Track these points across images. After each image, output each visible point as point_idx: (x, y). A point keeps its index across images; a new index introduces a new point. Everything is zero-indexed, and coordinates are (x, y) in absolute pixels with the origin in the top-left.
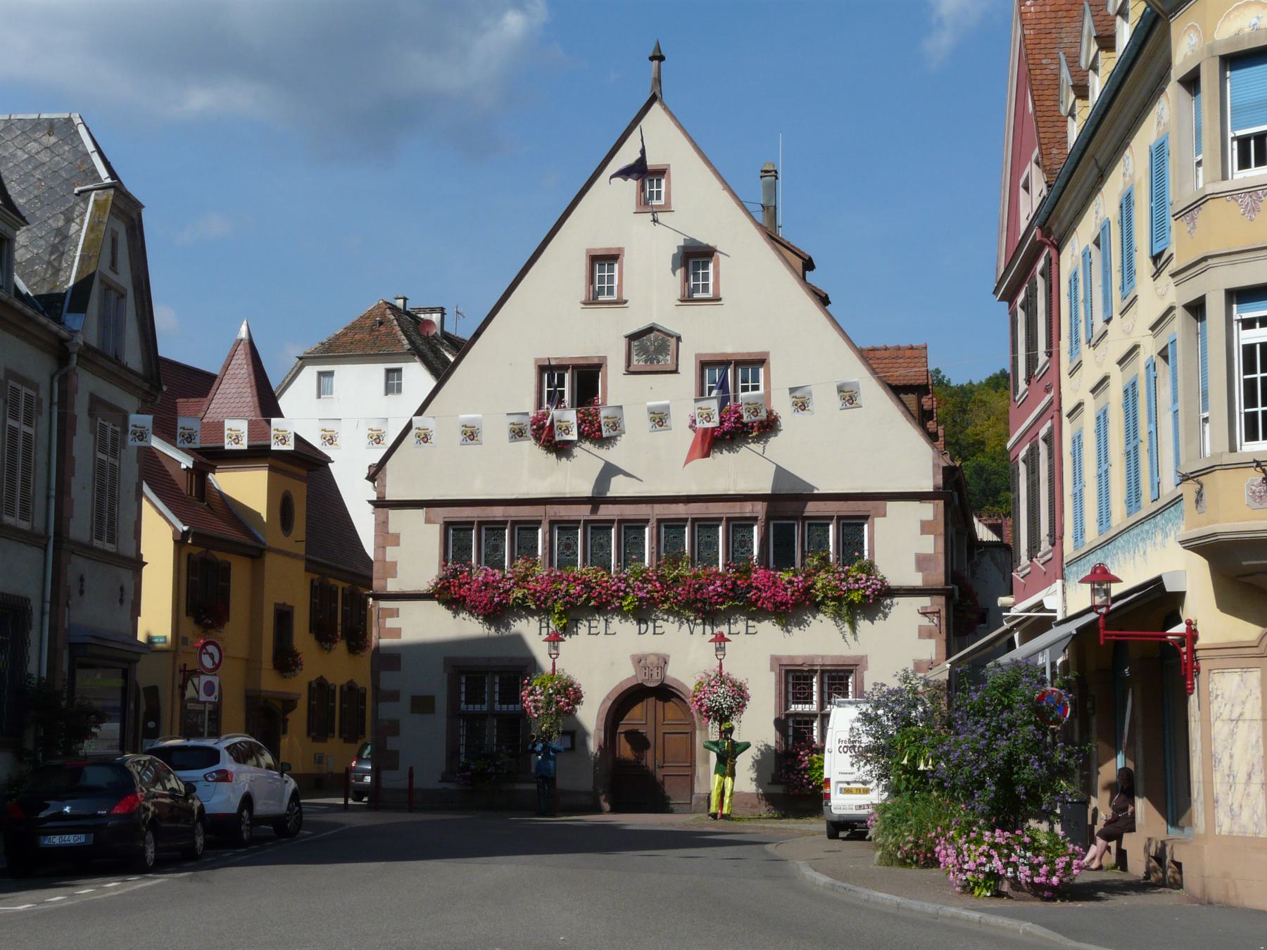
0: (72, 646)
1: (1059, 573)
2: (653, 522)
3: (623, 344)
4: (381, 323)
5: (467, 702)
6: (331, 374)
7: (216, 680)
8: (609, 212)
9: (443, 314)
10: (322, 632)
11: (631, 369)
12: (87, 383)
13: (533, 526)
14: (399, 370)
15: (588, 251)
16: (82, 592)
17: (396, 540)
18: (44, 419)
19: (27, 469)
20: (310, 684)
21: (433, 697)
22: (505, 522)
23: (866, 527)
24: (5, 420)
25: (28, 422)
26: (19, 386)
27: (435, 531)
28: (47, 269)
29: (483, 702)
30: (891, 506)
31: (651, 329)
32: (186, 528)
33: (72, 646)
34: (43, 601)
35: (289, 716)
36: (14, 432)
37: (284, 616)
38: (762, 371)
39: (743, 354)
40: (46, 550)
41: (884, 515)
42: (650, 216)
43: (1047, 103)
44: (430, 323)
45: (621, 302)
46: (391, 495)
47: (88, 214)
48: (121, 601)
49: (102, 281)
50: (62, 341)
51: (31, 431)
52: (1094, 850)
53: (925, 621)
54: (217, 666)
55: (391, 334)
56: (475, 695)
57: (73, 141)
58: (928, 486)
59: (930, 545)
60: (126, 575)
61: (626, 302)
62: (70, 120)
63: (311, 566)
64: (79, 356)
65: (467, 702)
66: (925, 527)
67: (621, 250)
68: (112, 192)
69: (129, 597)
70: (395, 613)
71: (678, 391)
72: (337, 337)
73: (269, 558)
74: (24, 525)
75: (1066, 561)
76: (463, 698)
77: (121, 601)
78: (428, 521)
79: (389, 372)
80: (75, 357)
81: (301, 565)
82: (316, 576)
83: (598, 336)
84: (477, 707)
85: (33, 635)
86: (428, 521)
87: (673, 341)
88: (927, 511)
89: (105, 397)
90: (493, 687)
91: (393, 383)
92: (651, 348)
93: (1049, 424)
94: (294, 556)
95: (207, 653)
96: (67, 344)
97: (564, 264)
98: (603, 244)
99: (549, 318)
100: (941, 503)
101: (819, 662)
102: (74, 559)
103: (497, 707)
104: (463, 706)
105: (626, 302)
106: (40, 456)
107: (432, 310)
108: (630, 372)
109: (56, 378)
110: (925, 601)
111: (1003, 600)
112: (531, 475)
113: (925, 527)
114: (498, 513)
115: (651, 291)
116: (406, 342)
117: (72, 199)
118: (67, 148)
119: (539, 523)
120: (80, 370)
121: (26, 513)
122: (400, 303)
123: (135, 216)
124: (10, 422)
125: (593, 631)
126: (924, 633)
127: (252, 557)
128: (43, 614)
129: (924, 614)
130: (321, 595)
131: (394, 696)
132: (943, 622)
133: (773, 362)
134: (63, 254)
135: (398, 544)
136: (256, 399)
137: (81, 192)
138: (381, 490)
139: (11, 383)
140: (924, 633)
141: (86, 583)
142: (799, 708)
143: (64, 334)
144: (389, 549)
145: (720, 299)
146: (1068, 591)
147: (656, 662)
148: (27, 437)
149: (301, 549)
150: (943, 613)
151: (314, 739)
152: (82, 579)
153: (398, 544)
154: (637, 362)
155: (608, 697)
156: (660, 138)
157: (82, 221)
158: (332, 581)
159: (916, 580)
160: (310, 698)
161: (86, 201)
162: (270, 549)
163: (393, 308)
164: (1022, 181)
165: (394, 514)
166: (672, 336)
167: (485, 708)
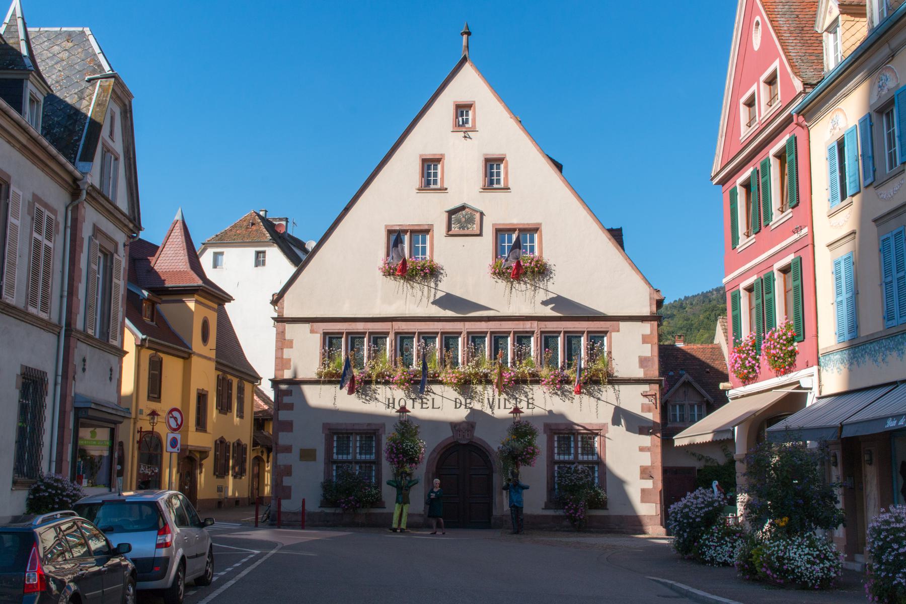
0: (77, 409)
1: (816, 362)
2: (464, 335)
3: (445, 215)
4: (253, 224)
5: (338, 454)
6: (222, 254)
7: (178, 437)
8: (433, 132)
9: (287, 222)
10: (224, 407)
11: (450, 233)
12: (91, 216)
13: (382, 336)
14: (264, 252)
15: (421, 156)
16: (84, 370)
17: (290, 344)
18: (59, 238)
19: (47, 273)
20: (216, 442)
21: (315, 450)
22: (365, 333)
23: (605, 339)
24: (31, 234)
25: (49, 238)
26: (43, 209)
27: (317, 339)
28: (64, 131)
29: (569, 454)
30: (622, 325)
31: (463, 208)
32: (144, 337)
33: (77, 409)
34: (56, 375)
35: (203, 462)
37: (202, 397)
38: (536, 236)
39: (528, 224)
40: (59, 337)
41: (618, 331)
42: (462, 134)
44: (280, 225)
45: (443, 189)
46: (287, 314)
47: (95, 94)
48: (111, 379)
49: (103, 144)
50: (75, 180)
51: (50, 245)
52: (737, 553)
53: (646, 401)
54: (179, 426)
58: (646, 311)
59: (649, 351)
60: (114, 359)
62: (83, 32)
63: (219, 366)
64: (87, 193)
65: (338, 454)
66: (645, 339)
67: (443, 155)
68: (113, 80)
69: (115, 376)
71: (482, 249)
73: (194, 359)
74: (44, 316)
75: (820, 352)
76: (335, 450)
77: (111, 379)
78: (312, 331)
79: (258, 253)
80: (84, 192)
81: (213, 365)
82: (220, 373)
83: (430, 211)
84: (345, 457)
85: (48, 400)
86: (312, 331)
87: (478, 216)
88: (647, 328)
89: (103, 229)
90: (356, 443)
91: (260, 259)
92: (461, 220)
94: (210, 359)
97: (404, 166)
100: (655, 323)
102: (79, 344)
103: (358, 457)
104: (335, 457)
106: (56, 265)
107: (281, 219)
109: (70, 208)
110: (646, 388)
111: (722, 386)
113: (645, 339)
114: (359, 327)
115: (462, 182)
117: (84, 84)
118: (80, 50)
119: (388, 333)
120: (86, 204)
121: (45, 307)
122: (262, 213)
123: (127, 103)
124: (35, 235)
125: (424, 406)
127: (183, 358)
128: (56, 384)
129: (646, 396)
130: (223, 387)
131: (288, 449)
132: (658, 401)
133: (544, 229)
134: (76, 121)
135: (291, 347)
136: (187, 257)
138: (280, 312)
139: (37, 205)
143: (78, 174)
144: (285, 350)
146: (823, 374)
148: (48, 249)
149: (213, 355)
150: (658, 396)
151: (218, 477)
152: (84, 360)
153: (291, 347)
156: (469, 84)
157: (91, 99)
158: (229, 377)
159: (640, 374)
160: (216, 451)
161: (94, 85)
162: (194, 353)
163: (259, 215)
165: (288, 327)
166: (477, 211)
167: (350, 457)
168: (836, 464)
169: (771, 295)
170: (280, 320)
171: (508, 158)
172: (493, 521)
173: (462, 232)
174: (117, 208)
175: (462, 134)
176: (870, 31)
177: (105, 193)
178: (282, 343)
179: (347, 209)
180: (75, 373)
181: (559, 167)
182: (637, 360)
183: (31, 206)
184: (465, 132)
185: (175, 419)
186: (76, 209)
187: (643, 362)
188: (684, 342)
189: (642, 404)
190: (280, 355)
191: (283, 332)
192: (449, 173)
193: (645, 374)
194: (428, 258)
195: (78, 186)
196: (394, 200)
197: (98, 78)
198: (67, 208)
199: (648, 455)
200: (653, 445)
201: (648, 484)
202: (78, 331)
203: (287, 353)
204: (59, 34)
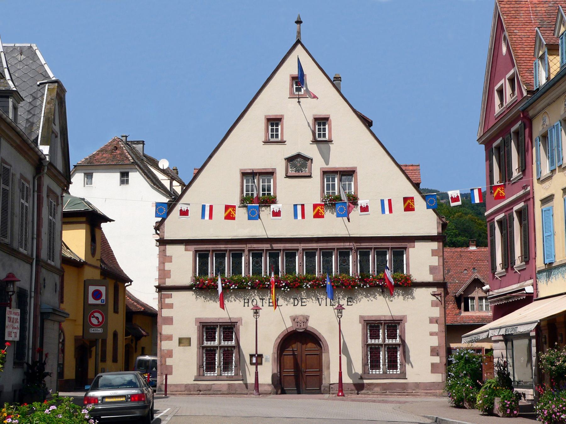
3: (284, 163)
8: (276, 97)
9: (144, 144)
11: (289, 174)
15: (265, 116)
17: (170, 259)
30: (418, 244)
36: (22, 204)
40: (32, 265)
43: (519, 51)
45: (283, 142)
46: (167, 237)
48: (56, 291)
53: (434, 298)
55: (122, 154)
56: (375, 335)
57: (34, 58)
61: (285, 142)
66: (434, 253)
67: (282, 116)
68: (56, 84)
70: (170, 296)
72: (94, 156)
77: (56, 291)
78: (186, 250)
80: (46, 168)
83: (274, 158)
86: (186, 250)
92: (298, 164)
93: (522, 204)
94: (96, 267)
95: (94, 317)
96: (43, 161)
97: (253, 125)
98: (273, 113)
99: (247, 148)
101: (383, 318)
105: (285, 142)
107: (138, 142)
108: (287, 177)
110: (435, 289)
112: (243, 227)
114: (222, 247)
115: (298, 137)
116: (130, 158)
122: (124, 139)
126: (434, 304)
129: (434, 295)
131: (170, 338)
137: (41, 84)
139: (22, 181)
140: (434, 304)
141: (46, 281)
142: (373, 341)
144: (166, 264)
145: (331, 141)
147: (303, 320)
152: (44, 280)
154: (291, 172)
155: (278, 337)
164: (499, 85)
168: (546, 344)
169: (526, 222)
170: (162, 242)
171: (331, 118)
172: (322, 388)
173: (297, 174)
174: (56, 169)
175: (297, 100)
176: (561, 67)
177: (55, 165)
178: (164, 258)
179: (211, 157)
180: (41, 289)
181: (368, 123)
182: (428, 269)
183: (20, 180)
184: (299, 98)
185: (97, 318)
186: (40, 180)
187: (432, 269)
188: (477, 246)
189: (432, 301)
190: (162, 268)
191: (164, 251)
192: (287, 130)
193: (434, 279)
194: (272, 194)
195: (42, 163)
196: (247, 148)
197: (46, 83)
198: (34, 178)
199: (436, 338)
200: (440, 331)
201: (436, 360)
202: (43, 261)
203: (168, 266)
204: (14, 48)
